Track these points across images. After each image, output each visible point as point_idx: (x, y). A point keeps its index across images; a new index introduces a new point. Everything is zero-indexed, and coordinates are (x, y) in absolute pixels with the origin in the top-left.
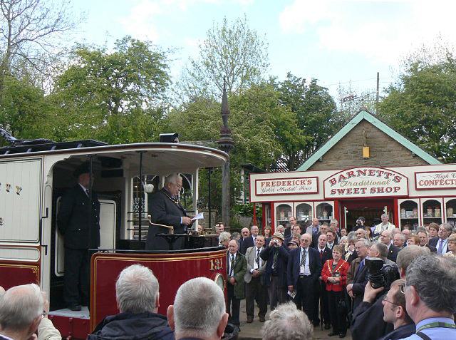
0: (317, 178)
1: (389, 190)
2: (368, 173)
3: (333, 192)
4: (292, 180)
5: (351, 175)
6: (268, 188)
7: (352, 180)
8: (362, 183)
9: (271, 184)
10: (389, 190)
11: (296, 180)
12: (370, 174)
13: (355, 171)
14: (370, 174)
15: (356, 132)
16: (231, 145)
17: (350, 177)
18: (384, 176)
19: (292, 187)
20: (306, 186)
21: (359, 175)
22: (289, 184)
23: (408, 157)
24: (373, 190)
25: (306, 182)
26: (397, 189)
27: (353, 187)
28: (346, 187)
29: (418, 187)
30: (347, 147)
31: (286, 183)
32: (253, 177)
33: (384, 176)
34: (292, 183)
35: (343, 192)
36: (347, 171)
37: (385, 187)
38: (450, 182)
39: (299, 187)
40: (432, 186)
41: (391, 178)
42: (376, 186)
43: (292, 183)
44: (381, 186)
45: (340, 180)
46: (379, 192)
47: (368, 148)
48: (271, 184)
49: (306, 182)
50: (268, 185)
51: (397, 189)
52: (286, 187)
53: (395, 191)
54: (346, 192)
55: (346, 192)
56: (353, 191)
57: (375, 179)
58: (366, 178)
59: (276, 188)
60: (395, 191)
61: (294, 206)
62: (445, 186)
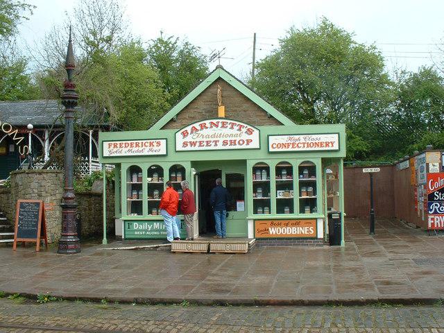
0: (166, 139)
1: (241, 142)
2: (220, 125)
3: (185, 144)
4: (140, 142)
5: (203, 127)
6: (115, 149)
7: (204, 132)
8: (214, 136)
9: (118, 146)
10: (241, 142)
11: (144, 141)
12: (223, 127)
13: (207, 122)
14: (223, 127)
15: (211, 90)
16: (75, 101)
17: (202, 129)
18: (236, 128)
19: (141, 149)
20: (155, 148)
21: (211, 127)
22: (137, 145)
23: (263, 118)
24: (225, 143)
25: (155, 144)
26: (249, 141)
27: (205, 140)
28: (198, 140)
29: (271, 150)
30: (202, 106)
31: (134, 145)
32: (102, 135)
33: (236, 128)
34: (140, 145)
35: (195, 145)
36: (200, 123)
37: (238, 139)
38: (302, 145)
39: (148, 148)
40: (284, 150)
41: (244, 130)
42: (229, 139)
43: (140, 145)
44: (233, 139)
45: (192, 132)
46: (231, 145)
47: (223, 99)
48: (118, 146)
49: (155, 144)
50: (115, 146)
51: (249, 141)
52: (135, 149)
53: (248, 144)
54: (198, 144)
55: (198, 144)
56: (205, 144)
57: (227, 131)
58: (218, 130)
59: (124, 150)
60: (248, 144)
61: (145, 167)
62: (297, 149)
